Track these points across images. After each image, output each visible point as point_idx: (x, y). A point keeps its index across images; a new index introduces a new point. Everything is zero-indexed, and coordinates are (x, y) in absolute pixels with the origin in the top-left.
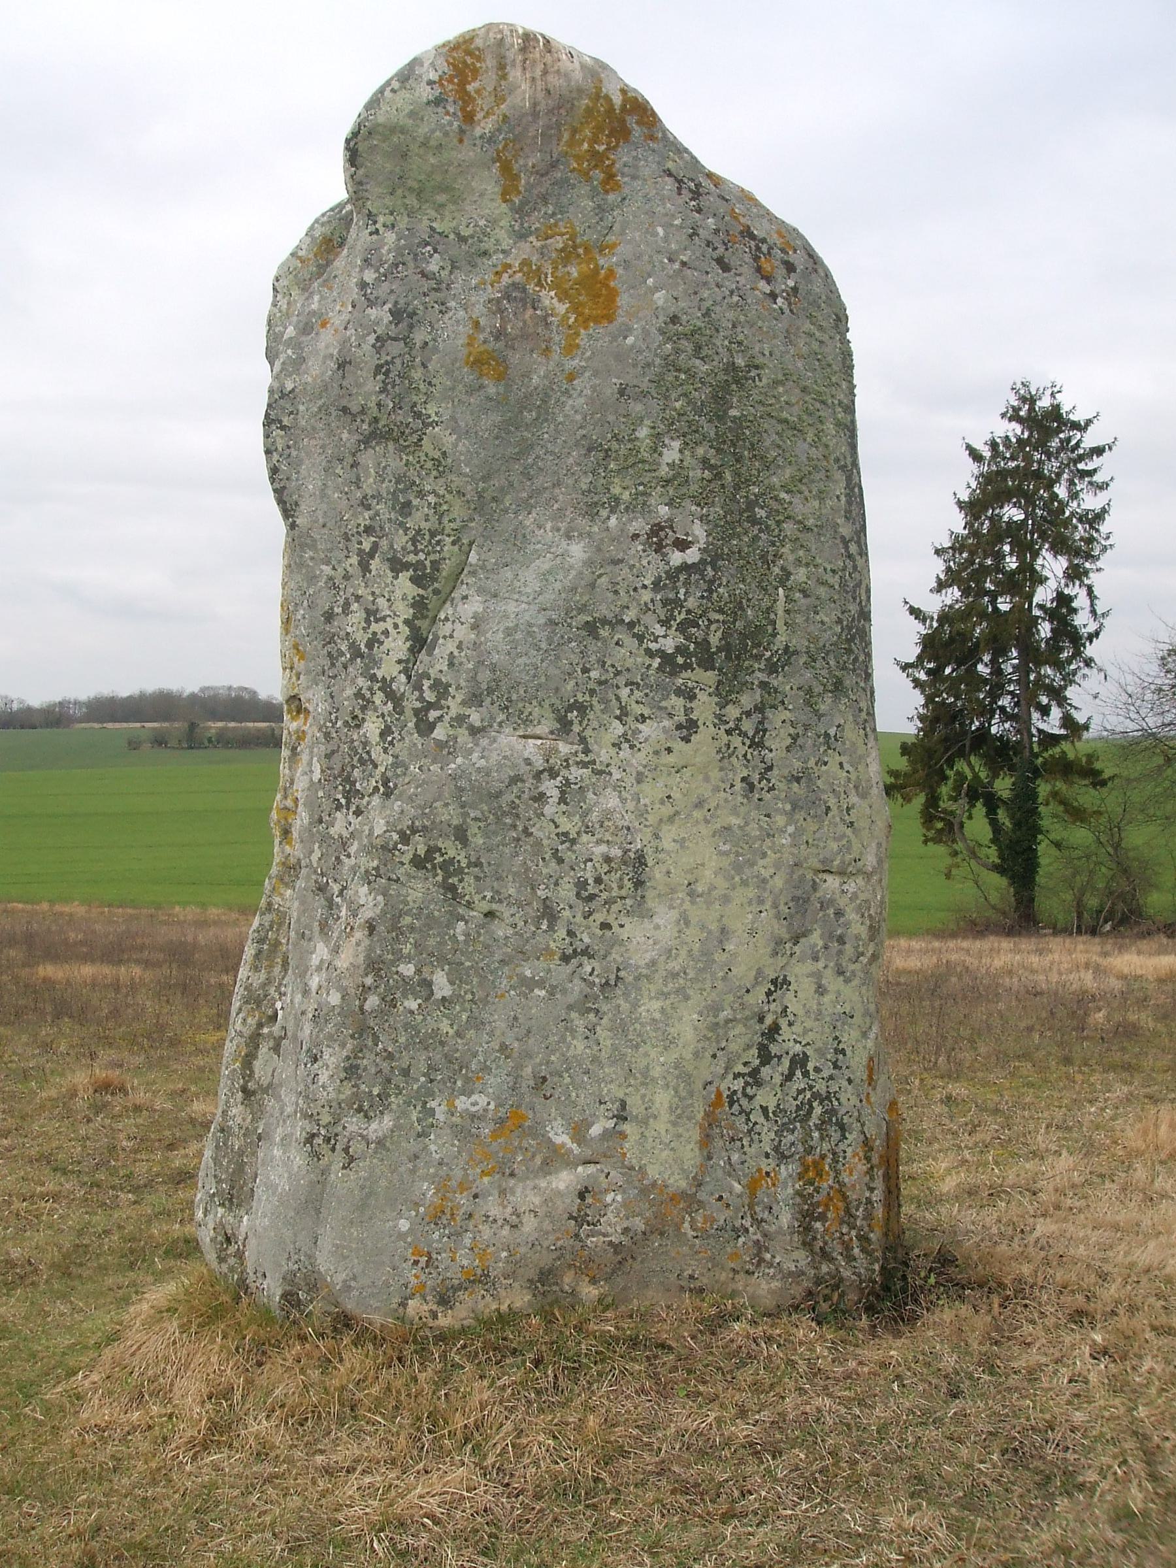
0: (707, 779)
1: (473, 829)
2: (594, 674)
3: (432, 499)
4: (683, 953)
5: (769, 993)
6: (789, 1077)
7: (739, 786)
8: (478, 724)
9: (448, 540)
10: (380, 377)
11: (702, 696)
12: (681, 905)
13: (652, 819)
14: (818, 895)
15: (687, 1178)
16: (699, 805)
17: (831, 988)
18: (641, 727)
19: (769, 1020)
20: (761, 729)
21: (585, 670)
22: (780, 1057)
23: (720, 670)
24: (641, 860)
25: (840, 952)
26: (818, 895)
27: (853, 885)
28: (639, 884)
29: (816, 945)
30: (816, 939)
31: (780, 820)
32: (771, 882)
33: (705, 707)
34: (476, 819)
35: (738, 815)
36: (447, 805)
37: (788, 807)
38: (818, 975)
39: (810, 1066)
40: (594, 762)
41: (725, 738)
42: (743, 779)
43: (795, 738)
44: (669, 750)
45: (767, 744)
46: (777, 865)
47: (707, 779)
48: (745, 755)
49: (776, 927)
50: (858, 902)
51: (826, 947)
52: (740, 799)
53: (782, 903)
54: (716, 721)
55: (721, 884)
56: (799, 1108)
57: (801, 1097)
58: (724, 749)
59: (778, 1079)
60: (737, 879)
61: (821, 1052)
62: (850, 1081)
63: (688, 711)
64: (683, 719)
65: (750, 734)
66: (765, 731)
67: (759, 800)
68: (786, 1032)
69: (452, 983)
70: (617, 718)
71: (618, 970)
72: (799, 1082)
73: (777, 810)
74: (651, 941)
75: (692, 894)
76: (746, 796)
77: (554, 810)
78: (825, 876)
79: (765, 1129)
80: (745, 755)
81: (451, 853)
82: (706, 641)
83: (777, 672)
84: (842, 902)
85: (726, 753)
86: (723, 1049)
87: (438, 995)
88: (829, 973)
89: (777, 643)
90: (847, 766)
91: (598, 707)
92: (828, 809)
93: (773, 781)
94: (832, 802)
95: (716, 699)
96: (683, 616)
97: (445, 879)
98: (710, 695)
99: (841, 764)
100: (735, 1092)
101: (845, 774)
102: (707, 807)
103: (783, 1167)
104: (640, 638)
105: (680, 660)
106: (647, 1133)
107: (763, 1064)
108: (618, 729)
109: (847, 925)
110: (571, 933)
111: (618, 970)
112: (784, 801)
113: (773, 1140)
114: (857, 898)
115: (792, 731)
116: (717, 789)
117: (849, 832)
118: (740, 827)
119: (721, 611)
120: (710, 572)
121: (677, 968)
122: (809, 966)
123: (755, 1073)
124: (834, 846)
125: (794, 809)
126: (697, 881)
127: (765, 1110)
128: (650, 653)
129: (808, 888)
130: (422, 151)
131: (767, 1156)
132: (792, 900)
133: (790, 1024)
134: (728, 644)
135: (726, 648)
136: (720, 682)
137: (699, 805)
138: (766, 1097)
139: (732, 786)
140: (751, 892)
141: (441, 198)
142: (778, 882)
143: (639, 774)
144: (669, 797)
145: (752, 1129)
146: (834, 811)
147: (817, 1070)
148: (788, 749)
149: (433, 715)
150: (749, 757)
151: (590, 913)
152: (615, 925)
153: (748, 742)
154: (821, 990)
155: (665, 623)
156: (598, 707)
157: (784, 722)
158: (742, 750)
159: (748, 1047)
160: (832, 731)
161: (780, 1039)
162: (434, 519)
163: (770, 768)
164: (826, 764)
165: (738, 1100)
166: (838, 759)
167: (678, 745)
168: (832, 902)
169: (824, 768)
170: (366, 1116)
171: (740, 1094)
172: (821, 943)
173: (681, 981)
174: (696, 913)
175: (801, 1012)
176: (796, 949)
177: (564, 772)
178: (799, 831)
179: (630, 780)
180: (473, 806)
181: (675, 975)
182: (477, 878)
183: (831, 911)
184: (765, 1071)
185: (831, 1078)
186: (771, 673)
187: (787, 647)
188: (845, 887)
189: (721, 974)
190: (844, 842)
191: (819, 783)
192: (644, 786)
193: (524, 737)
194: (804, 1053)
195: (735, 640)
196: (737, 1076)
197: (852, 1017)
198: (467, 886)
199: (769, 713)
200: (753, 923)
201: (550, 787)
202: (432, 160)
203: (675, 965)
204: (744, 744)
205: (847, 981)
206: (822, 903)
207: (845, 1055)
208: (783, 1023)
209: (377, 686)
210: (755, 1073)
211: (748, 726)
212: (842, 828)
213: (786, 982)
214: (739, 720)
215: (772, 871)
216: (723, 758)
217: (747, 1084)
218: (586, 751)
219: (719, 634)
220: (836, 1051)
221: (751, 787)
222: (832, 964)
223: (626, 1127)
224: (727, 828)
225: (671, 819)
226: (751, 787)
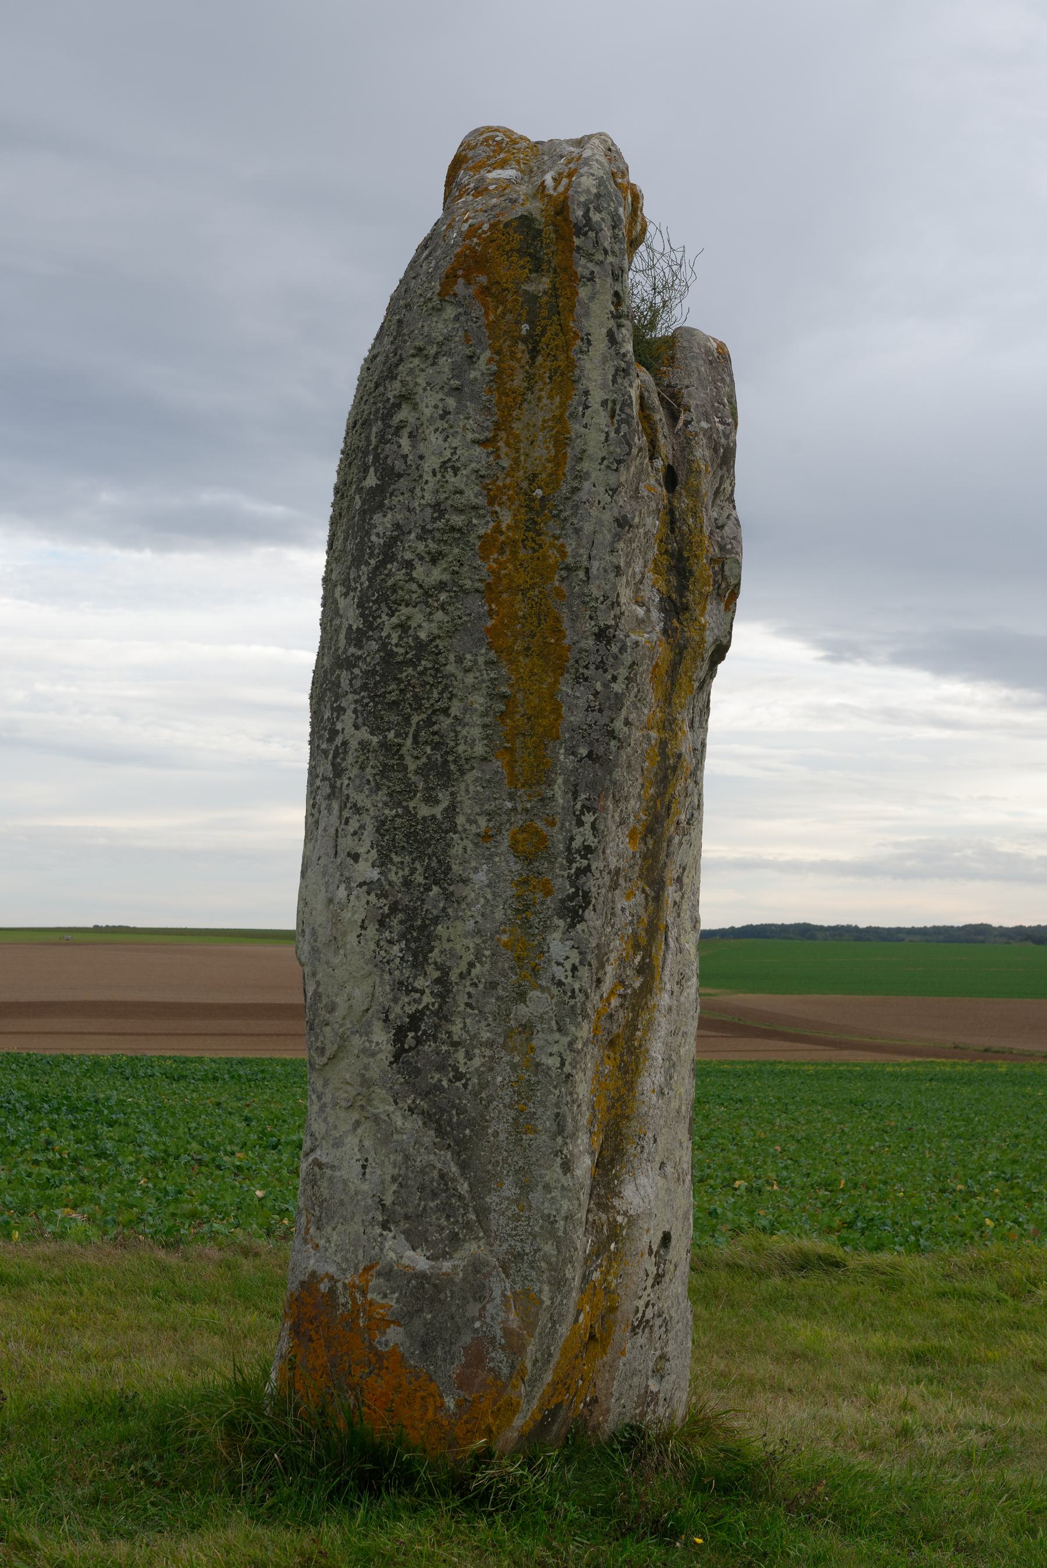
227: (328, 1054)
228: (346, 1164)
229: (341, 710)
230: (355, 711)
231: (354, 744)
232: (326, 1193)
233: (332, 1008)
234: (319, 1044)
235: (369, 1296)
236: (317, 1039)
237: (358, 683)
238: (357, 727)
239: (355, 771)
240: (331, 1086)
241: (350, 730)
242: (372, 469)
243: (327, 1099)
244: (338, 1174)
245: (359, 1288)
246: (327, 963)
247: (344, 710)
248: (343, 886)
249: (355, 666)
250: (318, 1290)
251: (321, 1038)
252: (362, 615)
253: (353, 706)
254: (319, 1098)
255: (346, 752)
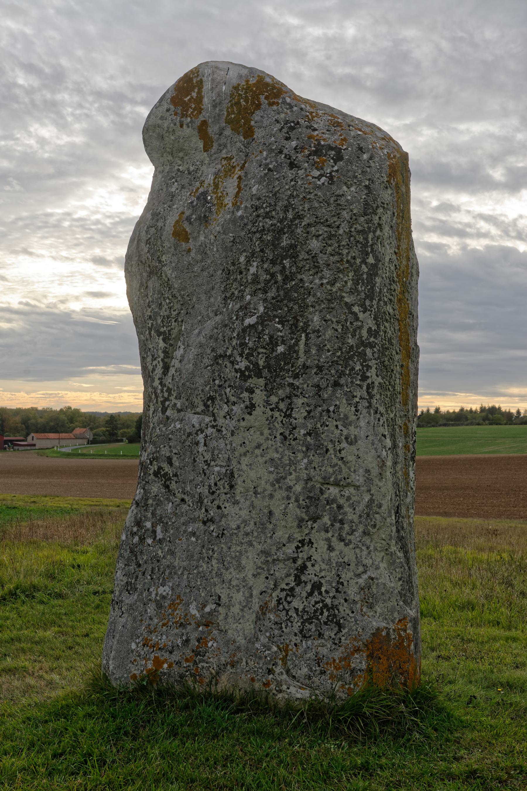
0: (262, 434)
1: (175, 459)
2: (217, 382)
3: (168, 301)
4: (252, 523)
5: (297, 548)
6: (310, 594)
7: (279, 437)
8: (179, 408)
9: (173, 320)
10: (148, 245)
11: (258, 391)
12: (251, 498)
13: (237, 454)
14: (325, 496)
15: (245, 639)
16: (258, 446)
17: (336, 548)
18: (234, 407)
19: (300, 562)
20: (290, 407)
21: (214, 380)
22: (306, 583)
23: (265, 378)
24: (232, 475)
25: (340, 529)
26: (325, 496)
27: (347, 492)
28: (232, 487)
29: (326, 524)
30: (326, 520)
31: (300, 456)
32: (294, 489)
33: (259, 396)
34: (176, 454)
35: (277, 452)
36: (165, 446)
37: (304, 449)
38: (328, 540)
39: (323, 589)
40: (217, 426)
41: (270, 413)
42: (281, 434)
43: (309, 412)
44: (243, 419)
45: (294, 416)
46: (298, 479)
47: (262, 434)
48: (282, 422)
49: (299, 512)
50: (351, 502)
51: (332, 525)
52: (279, 444)
53: (301, 499)
54: (265, 404)
55: (269, 487)
56: (315, 611)
57: (317, 606)
58: (270, 418)
59: (304, 594)
60: (277, 486)
61: (329, 582)
62: (346, 600)
63: (251, 399)
64: (248, 403)
65: (284, 410)
66: (292, 409)
67: (290, 445)
68: (310, 570)
69: (162, 532)
70: (226, 403)
71: (224, 530)
72: (316, 597)
73: (298, 451)
74: (237, 516)
75: (256, 493)
76: (282, 443)
77: (202, 449)
78: (328, 486)
79: (296, 620)
80: (282, 422)
81: (167, 470)
82: (257, 363)
83: (298, 377)
84: (341, 501)
85: (271, 420)
86: (272, 575)
87: (158, 538)
88: (334, 539)
89: (300, 363)
90: (340, 427)
91: (218, 398)
92: (327, 450)
93: (296, 435)
94: (330, 446)
95: (265, 393)
96: (247, 351)
97: (165, 482)
98: (261, 391)
99: (337, 427)
100: (281, 599)
101: (339, 431)
102: (262, 448)
103: (304, 642)
104: (232, 363)
105: (247, 373)
106: (229, 613)
107: (298, 585)
108: (226, 408)
109: (345, 514)
110: (206, 511)
111: (224, 530)
112: (302, 446)
113: (299, 627)
114: (351, 499)
115: (307, 409)
116: (267, 439)
117: (340, 463)
118: (279, 459)
119: (264, 348)
120: (260, 328)
121: (249, 530)
122: (323, 535)
123: (292, 589)
124: (331, 470)
125: (307, 450)
126: (258, 486)
127: (296, 610)
128: (236, 371)
129: (317, 492)
130: (167, 134)
131: (296, 635)
132: (307, 498)
133: (313, 565)
134: (268, 364)
135: (268, 366)
136: (266, 384)
137: (258, 446)
138: (296, 603)
139: (275, 437)
140: (285, 494)
141: (181, 154)
142: (298, 488)
143: (233, 431)
144: (244, 443)
145: (288, 619)
146: (331, 451)
147: (327, 592)
148: (305, 418)
149: (167, 403)
150: (284, 422)
151: (213, 500)
152: (223, 507)
153: (283, 415)
154: (331, 548)
155: (241, 355)
156: (218, 398)
157: (303, 404)
158: (280, 419)
159: (288, 575)
160: (332, 409)
161: (307, 573)
162: (168, 311)
163: (294, 428)
164: (327, 426)
165: (282, 603)
166: (335, 423)
167: (247, 417)
168: (334, 501)
169: (326, 428)
170: (129, 593)
171: (283, 600)
172: (329, 523)
173: (250, 537)
174: (258, 502)
175: (319, 560)
176: (315, 525)
177: (206, 430)
178: (310, 462)
179: (229, 435)
180: (175, 447)
181: (247, 534)
182: (176, 482)
183: (335, 506)
184: (298, 589)
185: (334, 597)
186: (295, 378)
187: (304, 364)
188: (343, 493)
189: (269, 535)
190: (337, 468)
191: (322, 436)
192: (234, 437)
193: (195, 413)
194: (320, 582)
195: (272, 362)
196: (283, 590)
197: (349, 565)
198: (173, 486)
199: (295, 400)
200: (285, 509)
201: (201, 438)
202: (173, 138)
203: (248, 529)
204: (281, 416)
205: (346, 545)
206: (328, 501)
207: (343, 585)
208: (309, 564)
209: (165, 389)
210: (292, 589)
211: (282, 406)
212: (335, 461)
213: (311, 543)
214: (278, 403)
215: (295, 482)
216: (270, 423)
217: (287, 595)
218: (215, 420)
219: (264, 359)
220: (338, 582)
221: (285, 438)
222: (336, 535)
223: (220, 609)
224: (272, 460)
225: (245, 454)
226: (285, 438)
227: (378, 527)
228: (383, 576)
229: (369, 367)
230: (376, 368)
231: (376, 384)
232: (375, 591)
233: (380, 506)
234: (373, 523)
235: (408, 632)
236: (371, 521)
237: (376, 355)
238: (377, 376)
239: (378, 397)
240: (374, 542)
241: (374, 377)
242: (371, 255)
243: (372, 548)
244: (380, 581)
245: (402, 630)
246: (377, 485)
247: (371, 367)
248: (384, 450)
249: (375, 347)
250: (381, 635)
251: (374, 520)
252: (376, 324)
253: (375, 366)
254: (368, 548)
255: (373, 387)
